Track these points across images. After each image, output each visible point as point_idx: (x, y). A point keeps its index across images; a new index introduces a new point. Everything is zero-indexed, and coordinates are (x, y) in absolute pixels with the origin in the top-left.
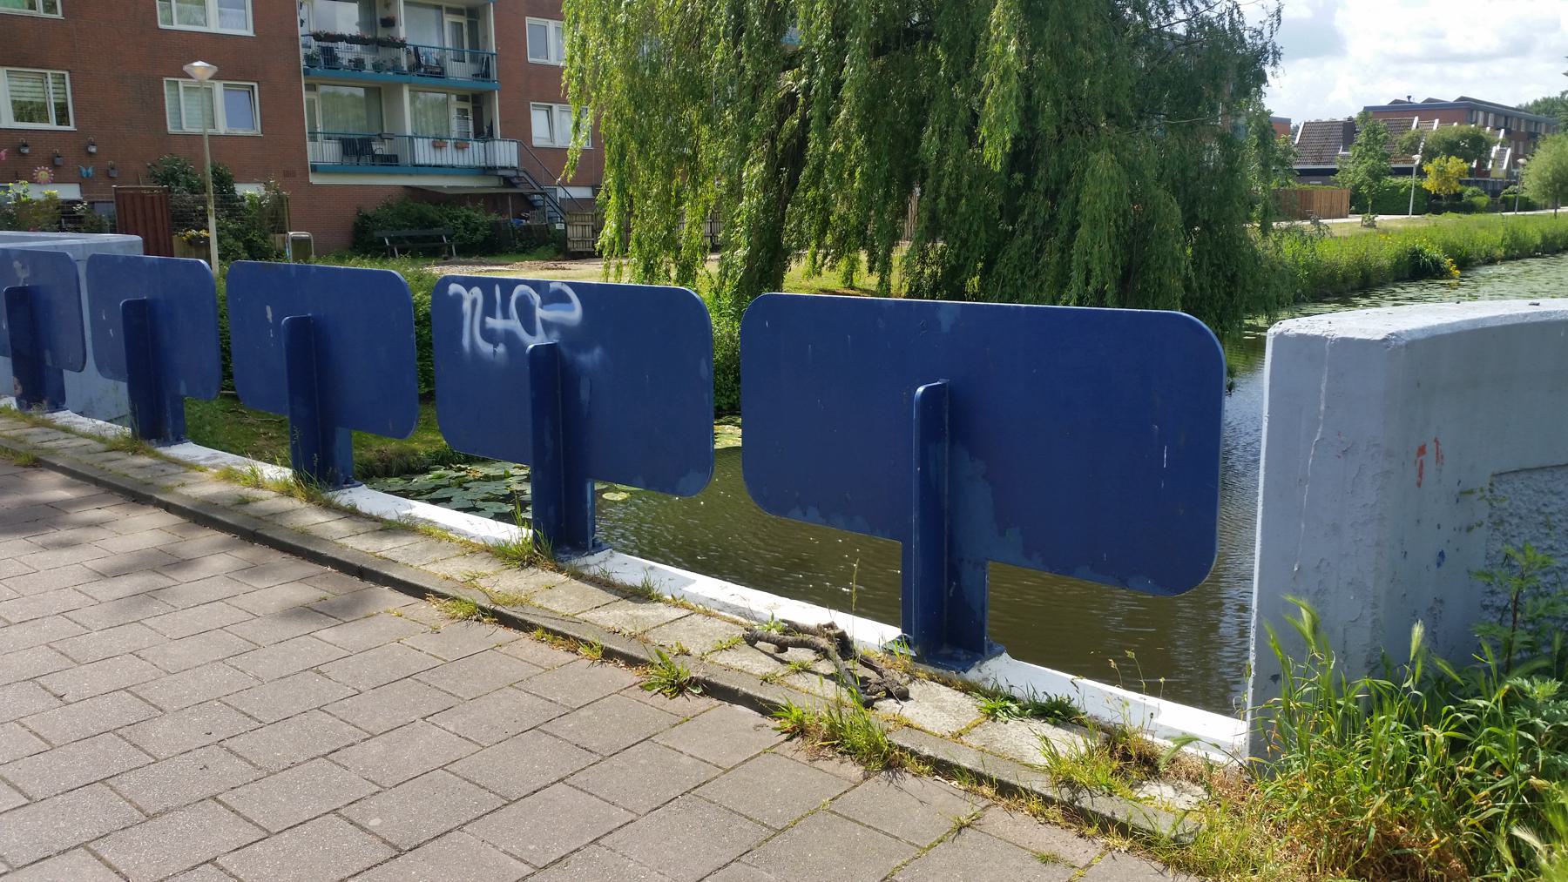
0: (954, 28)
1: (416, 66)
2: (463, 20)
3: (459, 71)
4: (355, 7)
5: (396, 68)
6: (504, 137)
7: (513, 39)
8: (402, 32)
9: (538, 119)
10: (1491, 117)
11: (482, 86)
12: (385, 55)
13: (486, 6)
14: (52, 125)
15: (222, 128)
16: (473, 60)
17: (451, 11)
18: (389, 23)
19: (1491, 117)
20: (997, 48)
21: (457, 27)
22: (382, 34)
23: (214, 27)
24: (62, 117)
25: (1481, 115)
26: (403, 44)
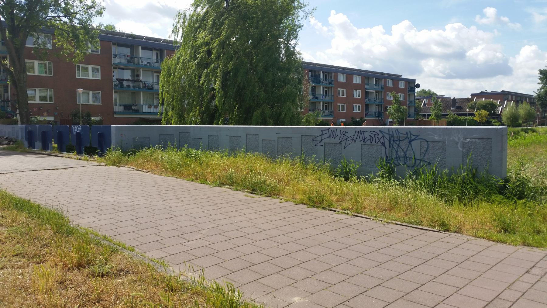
5: (139, 87)
8: (141, 78)
10: (514, 97)
12: (136, 84)
14: (48, 102)
15: (91, 103)
18: (138, 76)
19: (514, 97)
22: (136, 78)
24: (51, 101)
25: (510, 96)
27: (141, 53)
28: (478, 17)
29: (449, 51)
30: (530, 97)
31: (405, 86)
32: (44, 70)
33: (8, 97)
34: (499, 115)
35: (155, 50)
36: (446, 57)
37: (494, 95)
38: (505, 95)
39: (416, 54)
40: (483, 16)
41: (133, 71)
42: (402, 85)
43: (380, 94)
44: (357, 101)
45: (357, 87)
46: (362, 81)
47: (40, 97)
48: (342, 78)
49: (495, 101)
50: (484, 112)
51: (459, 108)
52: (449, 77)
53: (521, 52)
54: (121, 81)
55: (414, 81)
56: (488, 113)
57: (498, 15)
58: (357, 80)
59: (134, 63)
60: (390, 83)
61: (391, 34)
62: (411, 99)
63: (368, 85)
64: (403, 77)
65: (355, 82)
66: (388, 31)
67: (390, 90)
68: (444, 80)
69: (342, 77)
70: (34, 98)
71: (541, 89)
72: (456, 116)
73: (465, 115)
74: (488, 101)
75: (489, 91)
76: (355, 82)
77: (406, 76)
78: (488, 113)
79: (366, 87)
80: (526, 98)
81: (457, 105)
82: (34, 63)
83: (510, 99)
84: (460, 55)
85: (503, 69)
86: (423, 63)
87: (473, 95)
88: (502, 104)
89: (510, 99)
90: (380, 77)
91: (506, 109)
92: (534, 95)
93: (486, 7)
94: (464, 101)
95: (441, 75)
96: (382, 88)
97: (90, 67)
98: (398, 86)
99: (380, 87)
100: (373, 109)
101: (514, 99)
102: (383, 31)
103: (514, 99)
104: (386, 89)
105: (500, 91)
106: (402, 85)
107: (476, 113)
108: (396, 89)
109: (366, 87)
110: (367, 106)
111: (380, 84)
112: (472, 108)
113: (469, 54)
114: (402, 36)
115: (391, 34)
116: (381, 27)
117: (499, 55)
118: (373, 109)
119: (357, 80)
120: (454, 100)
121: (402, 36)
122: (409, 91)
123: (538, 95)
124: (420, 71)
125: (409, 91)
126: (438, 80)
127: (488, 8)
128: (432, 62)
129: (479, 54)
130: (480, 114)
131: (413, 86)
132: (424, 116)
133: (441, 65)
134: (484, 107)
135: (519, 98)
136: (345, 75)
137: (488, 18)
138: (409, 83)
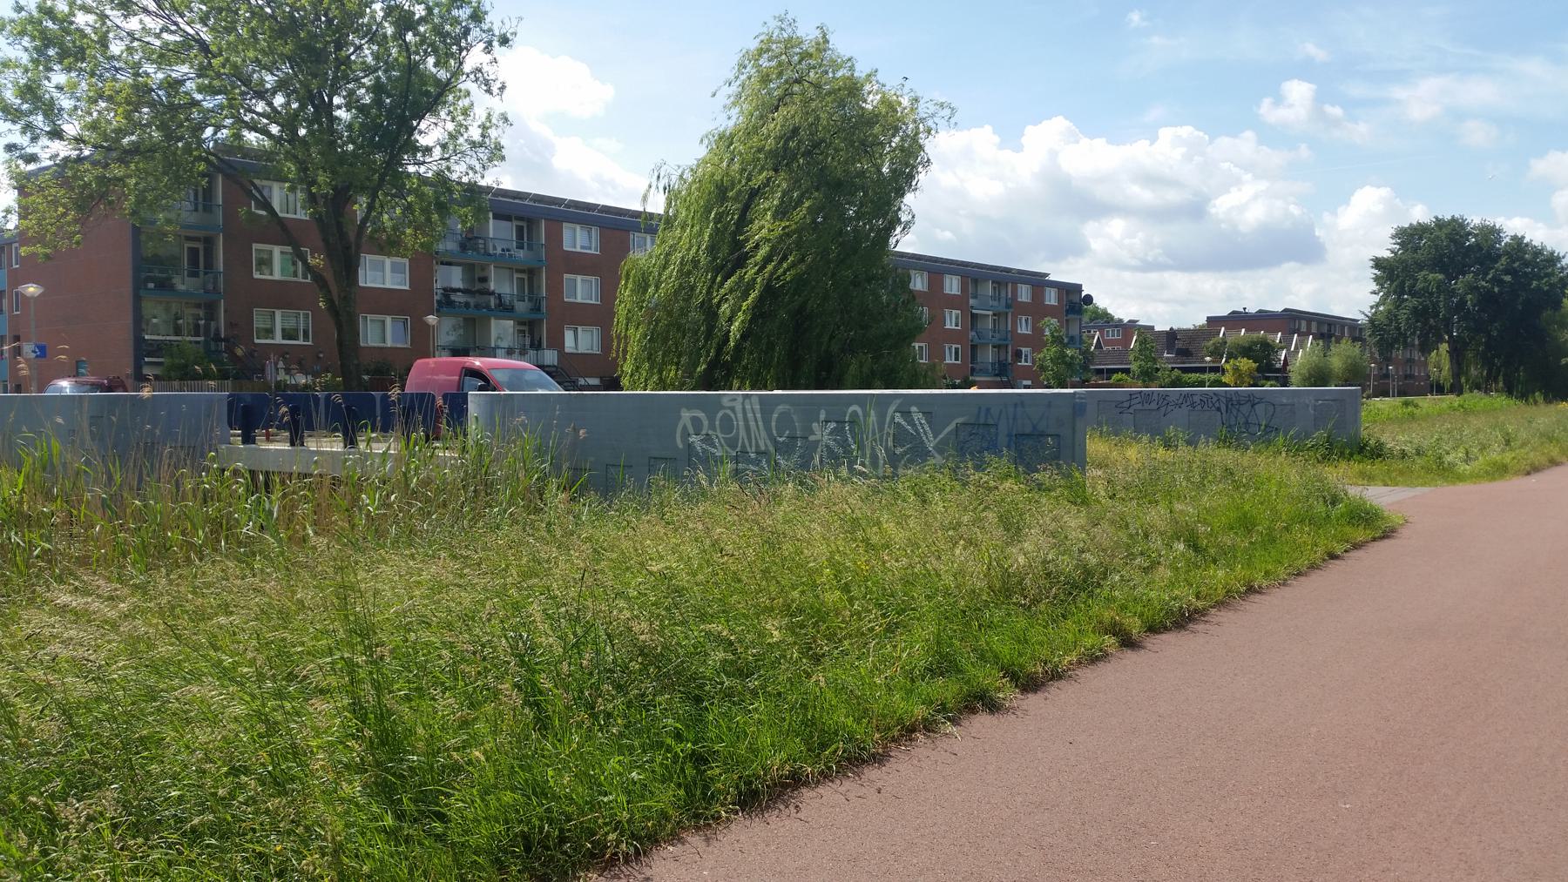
0: (295, 157)
1: (500, 304)
2: (525, 276)
3: (522, 307)
4: (988, 128)
5: (488, 307)
6: (549, 347)
7: (556, 288)
8: (492, 287)
9: (569, 337)
10: (1314, 325)
11: (534, 316)
12: (481, 299)
13: (540, 269)
14: (301, 342)
15: (389, 344)
16: (530, 300)
17: (518, 271)
18: (484, 280)
19: (1314, 325)
20: (251, 137)
21: (521, 280)
22: (478, 286)
23: (388, 286)
24: (306, 337)
25: (1304, 324)
26: (493, 293)
27: (493, 227)
28: (1267, 102)
29: (1172, 196)
30: (1352, 325)
31: (1060, 299)
32: (292, 269)
33: (217, 330)
34: (1278, 371)
35: (519, 218)
36: (1158, 215)
37: (1264, 319)
38: (1292, 321)
39: (1083, 203)
40: (1279, 100)
41: (469, 269)
42: (1051, 298)
43: (1002, 320)
44: (952, 336)
45: (952, 302)
46: (964, 288)
47: (283, 330)
48: (577, 240)
49: (1270, 337)
50: (1246, 364)
51: (1184, 353)
52: (1148, 266)
53: (1353, 199)
54: (448, 291)
55: (1078, 288)
56: (1255, 365)
57: (1320, 99)
58: (952, 285)
59: (476, 249)
60: (1024, 293)
61: (1019, 148)
62: (1071, 333)
63: (975, 297)
64: (1052, 278)
65: (947, 291)
66: (1011, 137)
67: (1023, 309)
68: (1139, 275)
69: (919, 280)
70: (270, 332)
71: (1378, 305)
72: (1177, 373)
73: (1202, 370)
74: (1255, 336)
75: (1252, 309)
76: (947, 291)
77: (1060, 273)
78: (1255, 365)
79: (972, 302)
80: (1343, 326)
81: (1179, 345)
82: (271, 252)
83: (1304, 329)
84: (1196, 210)
85: (1296, 246)
86: (1090, 228)
87: (1212, 321)
88: (1286, 342)
89: (1304, 329)
90: (1004, 278)
91: (1301, 354)
92: (1362, 319)
93: (1289, 78)
94: (1195, 335)
95: (1134, 262)
96: (1008, 306)
97: (388, 261)
98: (942, 288)
99: (1003, 302)
100: (989, 356)
101: (1314, 330)
102: (997, 139)
103: (1314, 330)
104: (1013, 305)
105: (1279, 308)
106: (1051, 298)
107: (1227, 366)
108: (1037, 309)
109: (972, 302)
110: (974, 347)
111: (1003, 294)
112: (1217, 353)
113: (1222, 206)
114: (1053, 154)
115: (1019, 148)
116: (988, 128)
117: (1295, 210)
118: (989, 356)
119: (952, 285)
120: (1172, 335)
121: (1053, 154)
122: (1068, 312)
123: (1372, 321)
124: (1078, 249)
125: (1068, 312)
126: (1127, 275)
127: (1296, 82)
128: (1116, 227)
129: (1247, 204)
130: (1236, 369)
131: (1076, 299)
132: (1100, 372)
133: (1140, 235)
134: (1246, 351)
135: (1327, 328)
136: (595, 231)
137: (1291, 106)
138: (1068, 292)
